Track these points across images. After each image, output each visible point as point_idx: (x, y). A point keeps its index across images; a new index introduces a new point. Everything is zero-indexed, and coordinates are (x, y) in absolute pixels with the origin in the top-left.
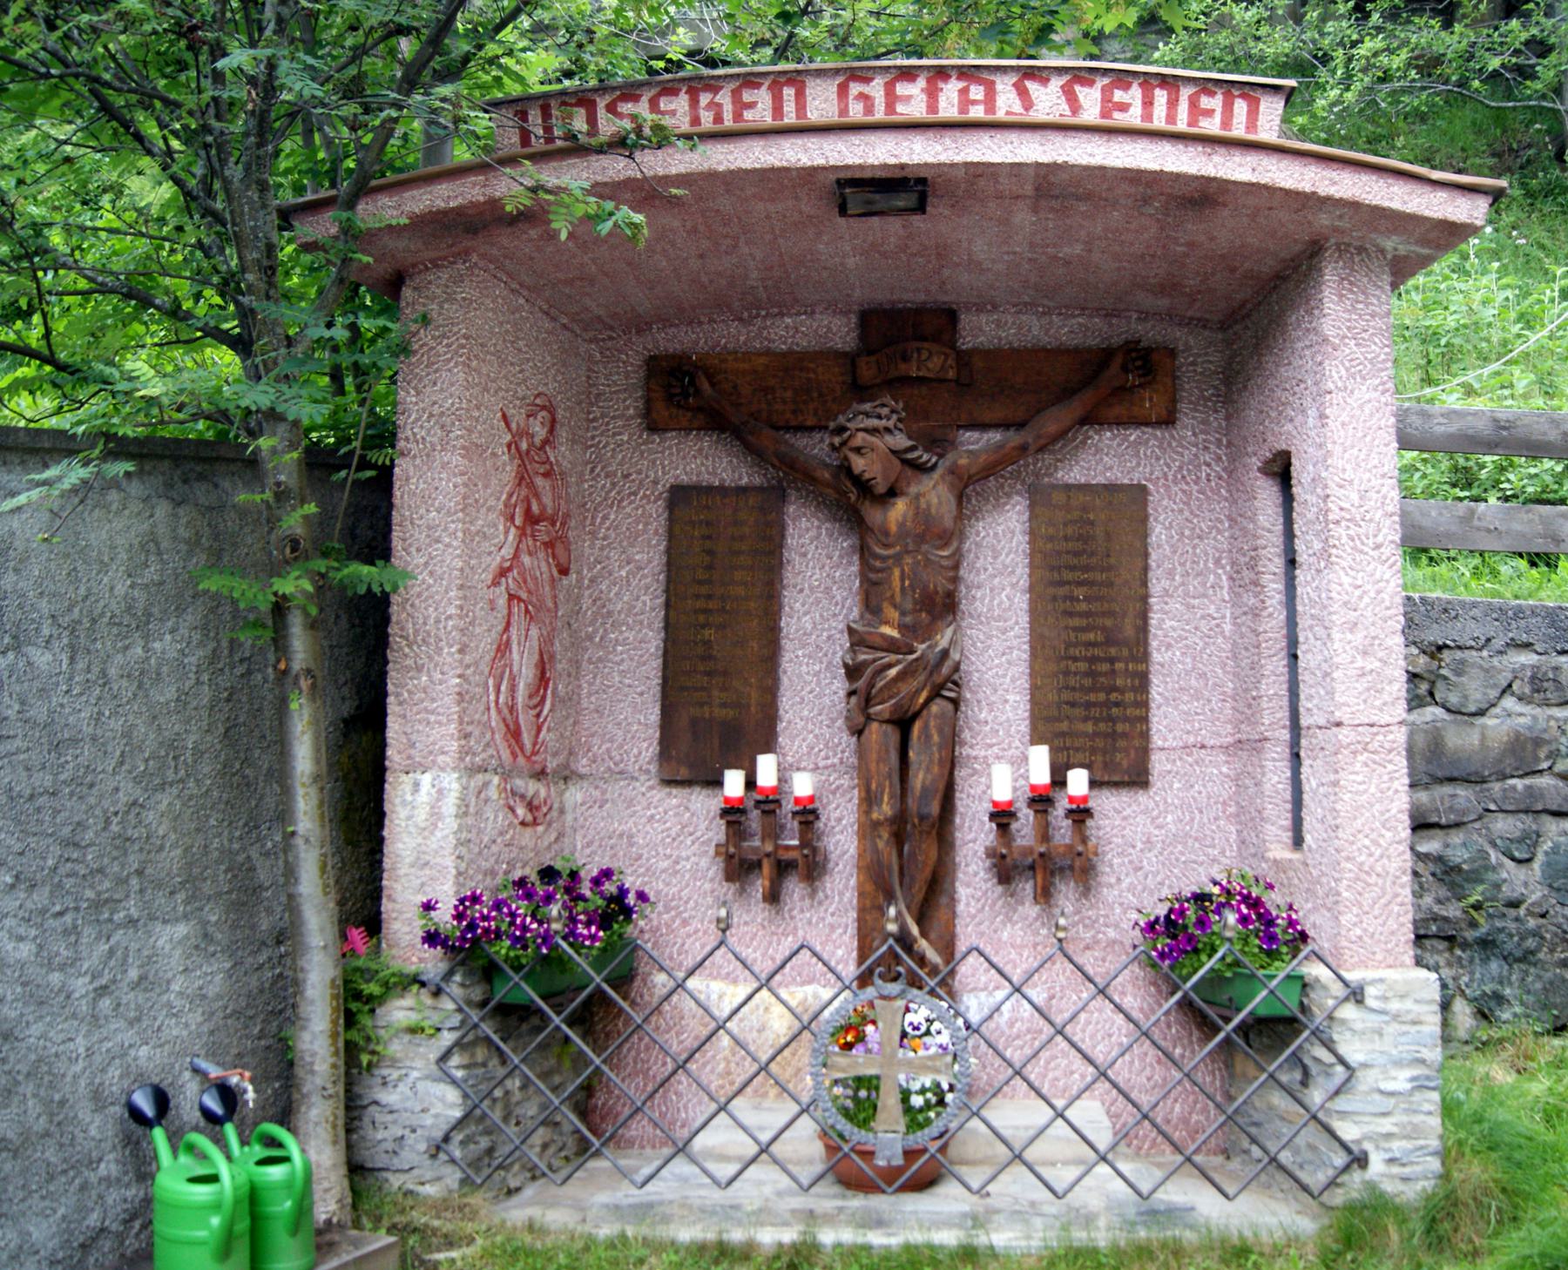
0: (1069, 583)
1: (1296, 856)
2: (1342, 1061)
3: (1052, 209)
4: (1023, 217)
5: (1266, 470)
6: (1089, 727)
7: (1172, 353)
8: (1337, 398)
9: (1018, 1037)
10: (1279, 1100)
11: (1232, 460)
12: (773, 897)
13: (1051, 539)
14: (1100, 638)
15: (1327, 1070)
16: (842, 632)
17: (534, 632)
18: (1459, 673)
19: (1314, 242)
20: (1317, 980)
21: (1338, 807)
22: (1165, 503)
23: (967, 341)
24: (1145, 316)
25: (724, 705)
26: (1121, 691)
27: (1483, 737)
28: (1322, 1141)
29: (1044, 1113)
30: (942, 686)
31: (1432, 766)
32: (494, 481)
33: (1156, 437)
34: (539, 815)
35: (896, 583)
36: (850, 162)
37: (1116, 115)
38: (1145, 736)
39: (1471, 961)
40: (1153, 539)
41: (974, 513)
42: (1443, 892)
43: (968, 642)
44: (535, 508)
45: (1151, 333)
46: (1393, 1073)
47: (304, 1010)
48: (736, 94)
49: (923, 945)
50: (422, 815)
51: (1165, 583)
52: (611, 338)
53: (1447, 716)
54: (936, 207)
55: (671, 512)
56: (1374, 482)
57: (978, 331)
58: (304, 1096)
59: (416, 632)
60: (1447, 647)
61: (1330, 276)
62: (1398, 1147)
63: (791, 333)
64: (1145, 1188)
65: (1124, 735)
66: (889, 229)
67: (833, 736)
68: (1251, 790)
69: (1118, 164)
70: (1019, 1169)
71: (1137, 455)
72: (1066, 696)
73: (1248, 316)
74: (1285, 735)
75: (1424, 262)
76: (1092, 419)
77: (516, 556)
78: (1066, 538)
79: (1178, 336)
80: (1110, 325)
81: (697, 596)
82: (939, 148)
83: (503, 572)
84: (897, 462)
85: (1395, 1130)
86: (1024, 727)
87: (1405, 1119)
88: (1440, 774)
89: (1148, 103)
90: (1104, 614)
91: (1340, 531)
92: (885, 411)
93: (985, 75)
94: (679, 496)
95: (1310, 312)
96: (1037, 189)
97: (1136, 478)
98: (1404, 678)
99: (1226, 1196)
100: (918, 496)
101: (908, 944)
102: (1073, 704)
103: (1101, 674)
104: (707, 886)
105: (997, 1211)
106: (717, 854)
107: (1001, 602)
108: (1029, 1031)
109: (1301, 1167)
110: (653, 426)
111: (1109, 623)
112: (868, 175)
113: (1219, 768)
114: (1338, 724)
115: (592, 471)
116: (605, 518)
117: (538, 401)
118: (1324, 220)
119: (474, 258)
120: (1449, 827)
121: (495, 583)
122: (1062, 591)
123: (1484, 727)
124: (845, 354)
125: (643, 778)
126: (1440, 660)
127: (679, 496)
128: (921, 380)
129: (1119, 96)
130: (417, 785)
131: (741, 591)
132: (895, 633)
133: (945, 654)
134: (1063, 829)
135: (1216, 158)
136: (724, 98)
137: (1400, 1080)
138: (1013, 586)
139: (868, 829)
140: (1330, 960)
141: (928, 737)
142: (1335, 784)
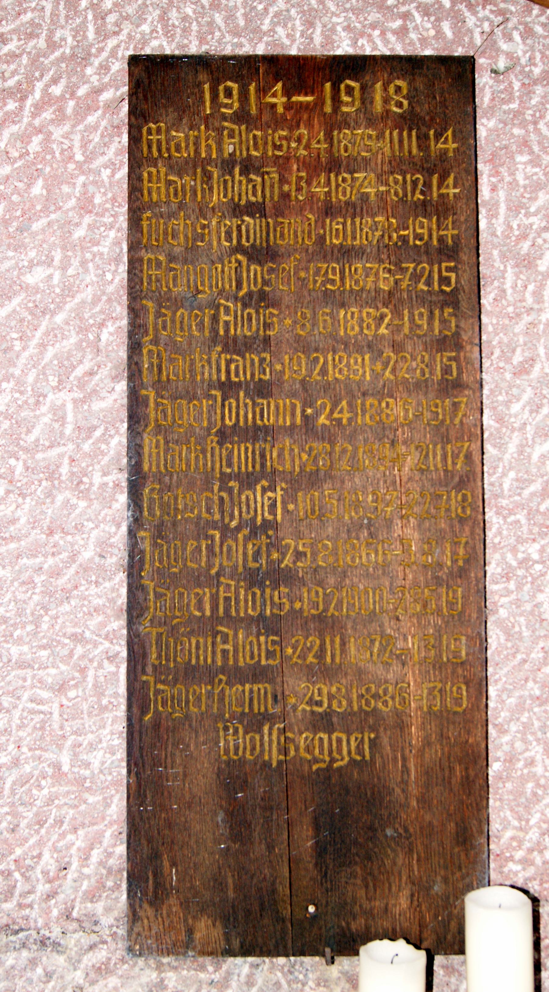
25: (323, 722)
81: (263, 390)
125: (75, 940)
131: (361, 368)
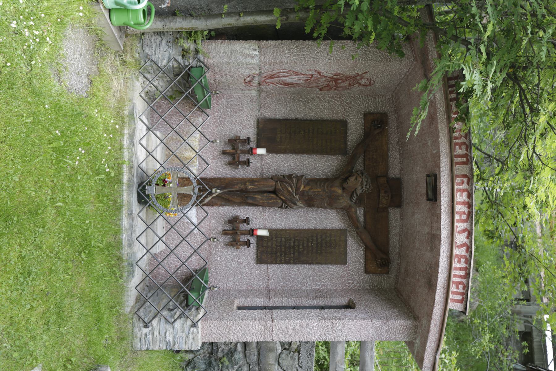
0: (317, 241)
1: (235, 307)
2: (175, 321)
3: (428, 239)
4: (426, 230)
5: (350, 301)
6: (274, 246)
7: (387, 273)
8: (370, 323)
9: (183, 225)
10: (165, 301)
11: (354, 291)
12: (224, 153)
14: (301, 250)
15: (172, 316)
16: (303, 173)
17: (302, 82)
18: (291, 357)
19: (418, 318)
20: (198, 313)
21: (248, 321)
23: (391, 211)
24: (399, 265)
26: (285, 256)
27: (272, 365)
28: (151, 315)
29: (160, 234)
30: (286, 203)
31: (262, 348)
32: (347, 70)
33: (361, 267)
34: (248, 84)
35: (316, 190)
36: (441, 179)
37: (456, 260)
38: (271, 263)
39: (205, 359)
40: (330, 266)
41: (338, 212)
42: (226, 351)
43: (299, 210)
44: (339, 81)
45: (394, 266)
46: (171, 336)
47: (189, 20)
48: (464, 143)
49: (210, 198)
50: (246, 51)
51: (317, 269)
52: (393, 102)
53: (278, 354)
54: (429, 204)
55: (339, 121)
56: (344, 334)
57: (394, 214)
58: (163, 19)
59: (301, 48)
60: (299, 354)
61: (408, 323)
62: (150, 337)
63: (394, 157)
64: (139, 263)
65: (272, 257)
66: (423, 189)
67: (272, 170)
68: (255, 294)
69: (441, 260)
70: (145, 227)
71: (356, 262)
72: (283, 239)
73: (398, 297)
74: (271, 305)
75: (412, 352)
76: (367, 249)
77: (324, 77)
78: (331, 240)
79: (393, 275)
80: (396, 254)
82: (446, 205)
83: (319, 73)
84: (353, 190)
85: (155, 336)
86: (274, 227)
87: (158, 339)
88: (261, 351)
89: (460, 269)
91: (329, 323)
92: (368, 187)
93: (470, 219)
94: (344, 124)
95: (397, 316)
96: (434, 235)
97: (349, 261)
98: (290, 341)
99: (137, 287)
100: (343, 196)
101: (211, 192)
104: (227, 133)
105: (133, 221)
106: (237, 136)
108: (185, 228)
109: (145, 308)
110: (366, 115)
111: (305, 253)
112: (438, 184)
113: (262, 285)
114: (272, 321)
115: (352, 97)
116: (338, 101)
117: (372, 81)
118: (424, 321)
119: (415, 63)
120: (245, 353)
121: (316, 71)
123: (275, 365)
124: (387, 174)
126: (295, 352)
127: (344, 124)
128: (379, 197)
129: (463, 260)
130: (255, 50)
132: (301, 189)
133: (296, 204)
134: (243, 238)
135: (442, 290)
136: (463, 140)
137: (169, 338)
138: (316, 224)
139: (244, 181)
140: (204, 317)
141: (271, 199)
142: (255, 320)
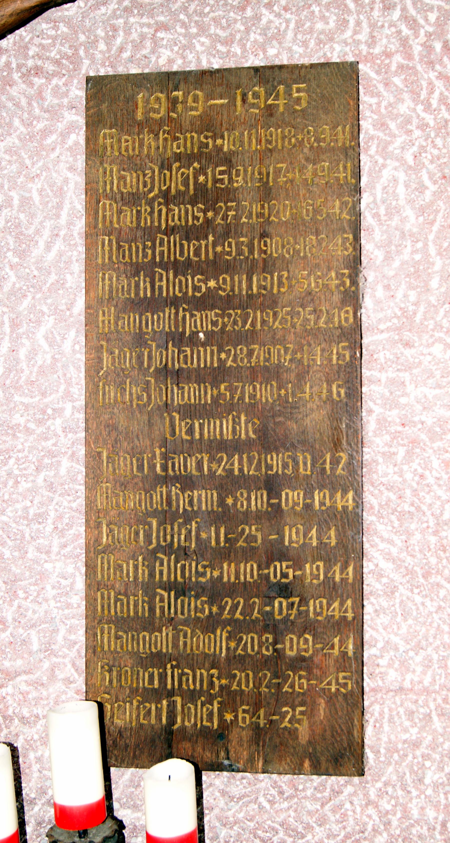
0: (174, 302)
6: (219, 643)
13: (132, 199)
14: (246, 430)
22: (403, 109)
65: (300, 663)
72: (166, 568)
90: (254, 374)
102: (181, 590)
103: (247, 518)
107: (33, 353)
111: (265, 394)
122: (162, 321)
